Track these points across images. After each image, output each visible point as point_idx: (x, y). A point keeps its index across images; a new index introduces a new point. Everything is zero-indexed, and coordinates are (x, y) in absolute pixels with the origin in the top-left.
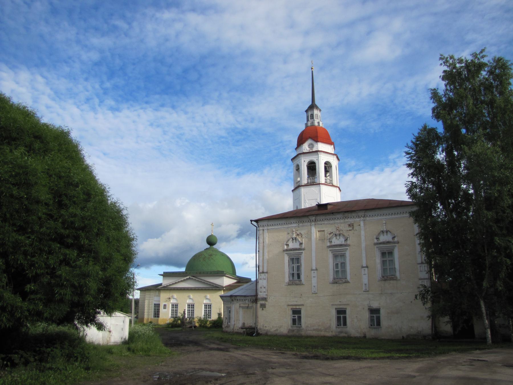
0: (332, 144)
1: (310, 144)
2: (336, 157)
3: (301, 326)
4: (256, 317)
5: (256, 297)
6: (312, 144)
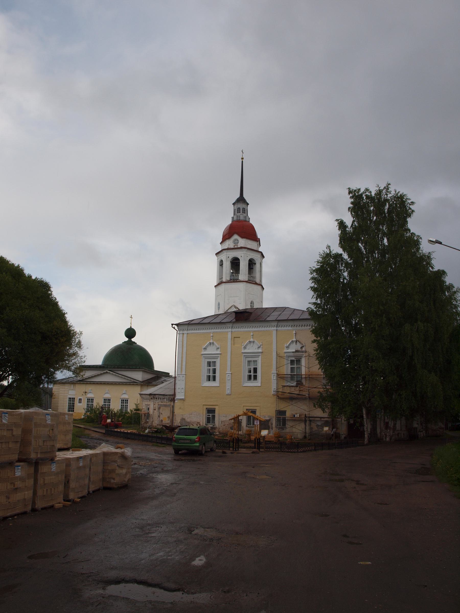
0: (257, 241)
1: (235, 240)
2: (261, 254)
3: (215, 425)
4: (153, 472)
5: (174, 396)
6: (237, 240)
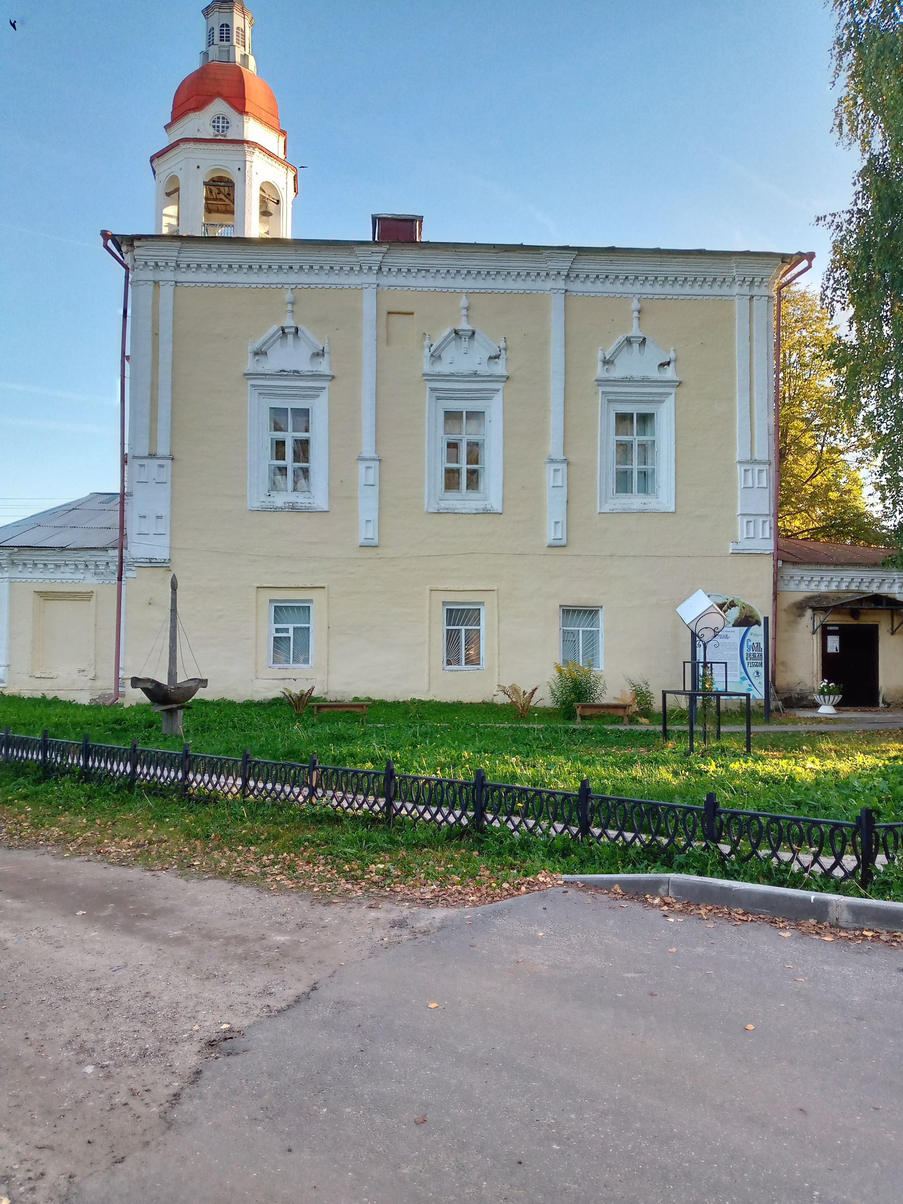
1: (219, 118)
6: (223, 118)
